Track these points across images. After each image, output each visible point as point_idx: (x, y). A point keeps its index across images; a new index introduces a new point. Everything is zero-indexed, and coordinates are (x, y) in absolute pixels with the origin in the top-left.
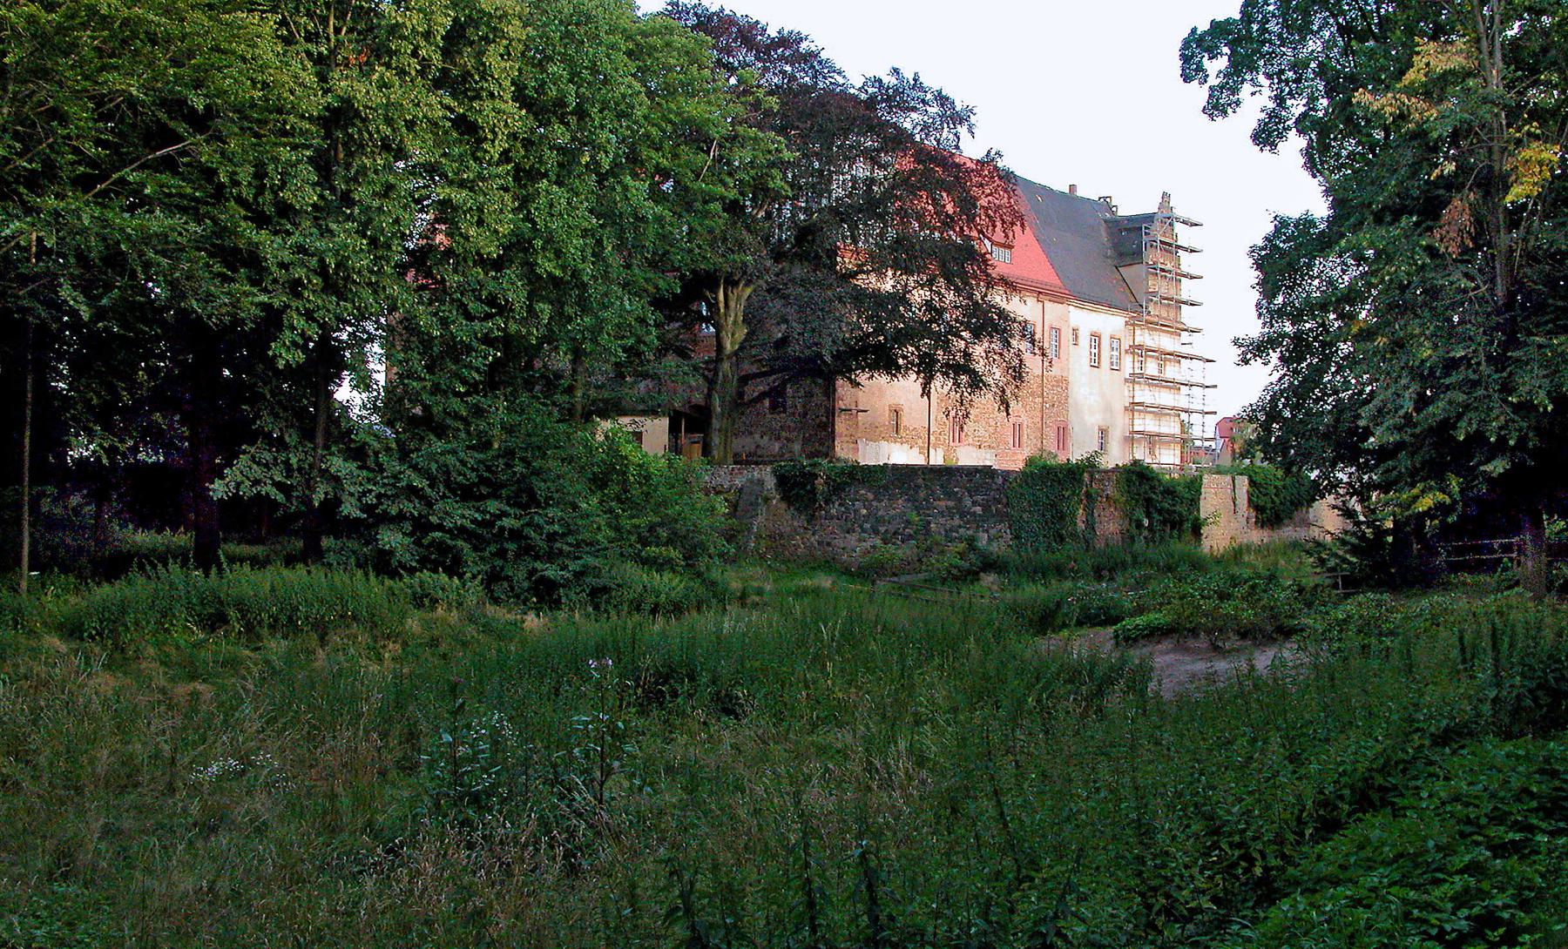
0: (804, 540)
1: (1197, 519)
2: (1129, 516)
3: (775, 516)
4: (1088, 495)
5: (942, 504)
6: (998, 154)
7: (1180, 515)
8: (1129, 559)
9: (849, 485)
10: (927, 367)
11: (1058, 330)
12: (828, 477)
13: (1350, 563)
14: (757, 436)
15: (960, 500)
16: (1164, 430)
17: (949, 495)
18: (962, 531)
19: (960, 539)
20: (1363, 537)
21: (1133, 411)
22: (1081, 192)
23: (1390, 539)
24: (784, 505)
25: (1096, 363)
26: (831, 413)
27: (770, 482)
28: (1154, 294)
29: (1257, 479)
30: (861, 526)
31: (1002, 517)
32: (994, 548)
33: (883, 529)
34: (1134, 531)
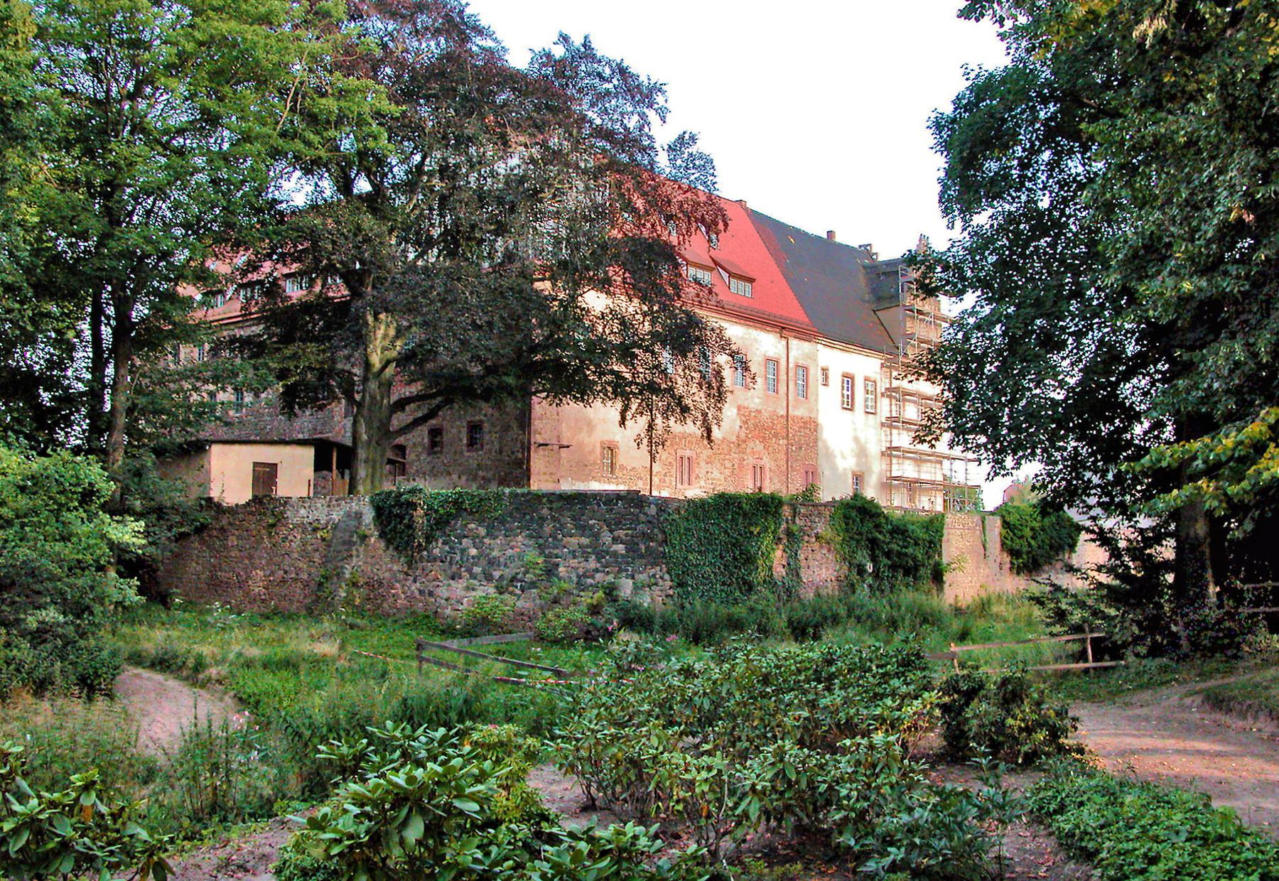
0: (404, 592)
1: (938, 564)
2: (848, 559)
3: (374, 559)
4: (789, 533)
5: (574, 540)
6: (693, 139)
7: (914, 558)
8: (842, 611)
9: (456, 517)
10: (619, 389)
11: (805, 369)
12: (430, 508)
13: (1105, 617)
14: (455, 477)
15: (596, 536)
16: (925, 476)
17: (583, 529)
18: (599, 576)
19: (596, 587)
20: (1125, 577)
21: (890, 456)
22: (839, 239)
23: (1170, 578)
24: (382, 544)
25: (849, 405)
26: (526, 448)
27: (369, 515)
28: (911, 336)
29: (1011, 519)
30: (469, 571)
31: (654, 558)
32: (645, 600)
33: (497, 574)
34: (855, 577)
